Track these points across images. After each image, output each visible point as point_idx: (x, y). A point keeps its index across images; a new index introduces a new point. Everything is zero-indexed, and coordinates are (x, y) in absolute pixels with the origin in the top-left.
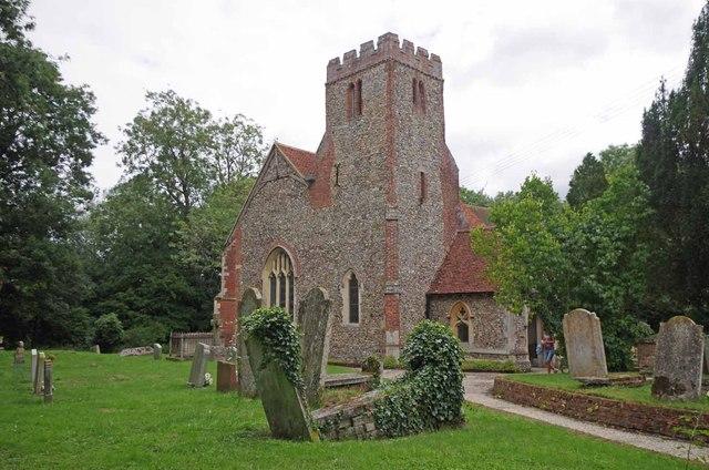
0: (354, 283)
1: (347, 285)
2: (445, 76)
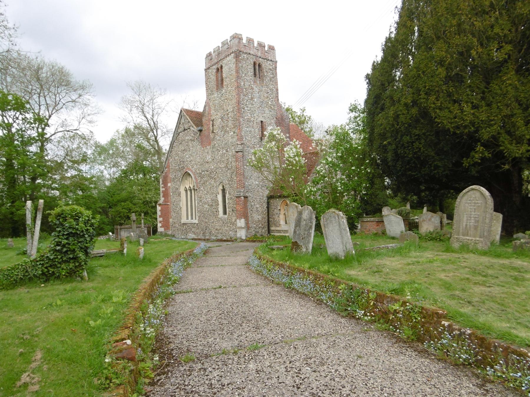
0: (224, 190)
2: (277, 59)
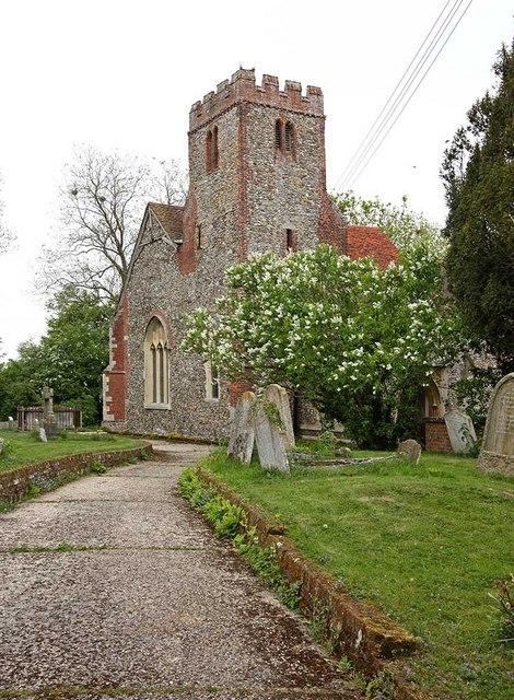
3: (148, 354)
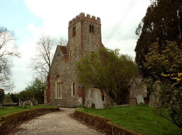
0: (74, 84)
1: (72, 84)
3: (56, 84)
